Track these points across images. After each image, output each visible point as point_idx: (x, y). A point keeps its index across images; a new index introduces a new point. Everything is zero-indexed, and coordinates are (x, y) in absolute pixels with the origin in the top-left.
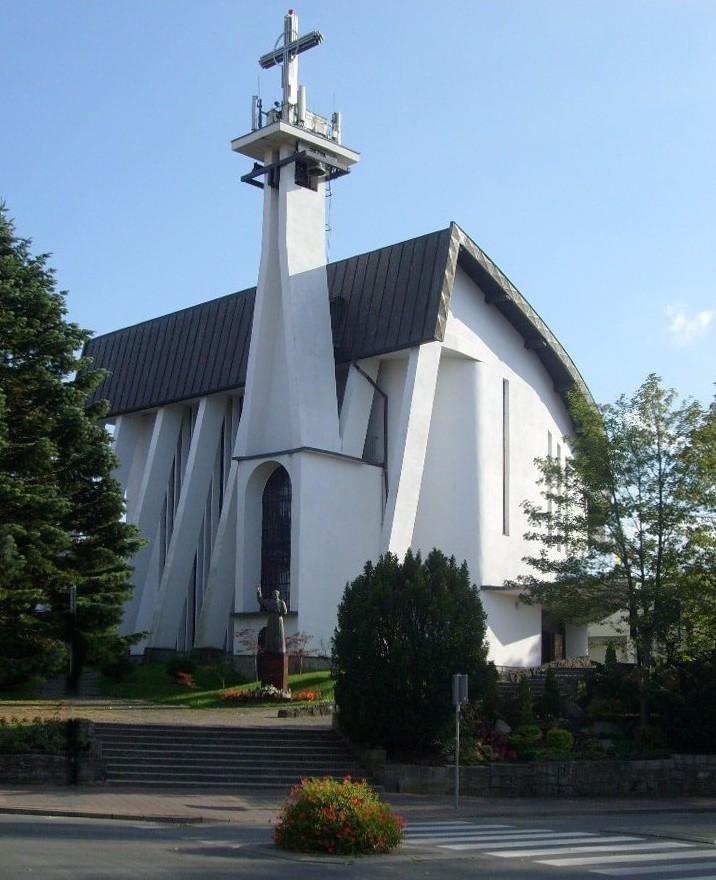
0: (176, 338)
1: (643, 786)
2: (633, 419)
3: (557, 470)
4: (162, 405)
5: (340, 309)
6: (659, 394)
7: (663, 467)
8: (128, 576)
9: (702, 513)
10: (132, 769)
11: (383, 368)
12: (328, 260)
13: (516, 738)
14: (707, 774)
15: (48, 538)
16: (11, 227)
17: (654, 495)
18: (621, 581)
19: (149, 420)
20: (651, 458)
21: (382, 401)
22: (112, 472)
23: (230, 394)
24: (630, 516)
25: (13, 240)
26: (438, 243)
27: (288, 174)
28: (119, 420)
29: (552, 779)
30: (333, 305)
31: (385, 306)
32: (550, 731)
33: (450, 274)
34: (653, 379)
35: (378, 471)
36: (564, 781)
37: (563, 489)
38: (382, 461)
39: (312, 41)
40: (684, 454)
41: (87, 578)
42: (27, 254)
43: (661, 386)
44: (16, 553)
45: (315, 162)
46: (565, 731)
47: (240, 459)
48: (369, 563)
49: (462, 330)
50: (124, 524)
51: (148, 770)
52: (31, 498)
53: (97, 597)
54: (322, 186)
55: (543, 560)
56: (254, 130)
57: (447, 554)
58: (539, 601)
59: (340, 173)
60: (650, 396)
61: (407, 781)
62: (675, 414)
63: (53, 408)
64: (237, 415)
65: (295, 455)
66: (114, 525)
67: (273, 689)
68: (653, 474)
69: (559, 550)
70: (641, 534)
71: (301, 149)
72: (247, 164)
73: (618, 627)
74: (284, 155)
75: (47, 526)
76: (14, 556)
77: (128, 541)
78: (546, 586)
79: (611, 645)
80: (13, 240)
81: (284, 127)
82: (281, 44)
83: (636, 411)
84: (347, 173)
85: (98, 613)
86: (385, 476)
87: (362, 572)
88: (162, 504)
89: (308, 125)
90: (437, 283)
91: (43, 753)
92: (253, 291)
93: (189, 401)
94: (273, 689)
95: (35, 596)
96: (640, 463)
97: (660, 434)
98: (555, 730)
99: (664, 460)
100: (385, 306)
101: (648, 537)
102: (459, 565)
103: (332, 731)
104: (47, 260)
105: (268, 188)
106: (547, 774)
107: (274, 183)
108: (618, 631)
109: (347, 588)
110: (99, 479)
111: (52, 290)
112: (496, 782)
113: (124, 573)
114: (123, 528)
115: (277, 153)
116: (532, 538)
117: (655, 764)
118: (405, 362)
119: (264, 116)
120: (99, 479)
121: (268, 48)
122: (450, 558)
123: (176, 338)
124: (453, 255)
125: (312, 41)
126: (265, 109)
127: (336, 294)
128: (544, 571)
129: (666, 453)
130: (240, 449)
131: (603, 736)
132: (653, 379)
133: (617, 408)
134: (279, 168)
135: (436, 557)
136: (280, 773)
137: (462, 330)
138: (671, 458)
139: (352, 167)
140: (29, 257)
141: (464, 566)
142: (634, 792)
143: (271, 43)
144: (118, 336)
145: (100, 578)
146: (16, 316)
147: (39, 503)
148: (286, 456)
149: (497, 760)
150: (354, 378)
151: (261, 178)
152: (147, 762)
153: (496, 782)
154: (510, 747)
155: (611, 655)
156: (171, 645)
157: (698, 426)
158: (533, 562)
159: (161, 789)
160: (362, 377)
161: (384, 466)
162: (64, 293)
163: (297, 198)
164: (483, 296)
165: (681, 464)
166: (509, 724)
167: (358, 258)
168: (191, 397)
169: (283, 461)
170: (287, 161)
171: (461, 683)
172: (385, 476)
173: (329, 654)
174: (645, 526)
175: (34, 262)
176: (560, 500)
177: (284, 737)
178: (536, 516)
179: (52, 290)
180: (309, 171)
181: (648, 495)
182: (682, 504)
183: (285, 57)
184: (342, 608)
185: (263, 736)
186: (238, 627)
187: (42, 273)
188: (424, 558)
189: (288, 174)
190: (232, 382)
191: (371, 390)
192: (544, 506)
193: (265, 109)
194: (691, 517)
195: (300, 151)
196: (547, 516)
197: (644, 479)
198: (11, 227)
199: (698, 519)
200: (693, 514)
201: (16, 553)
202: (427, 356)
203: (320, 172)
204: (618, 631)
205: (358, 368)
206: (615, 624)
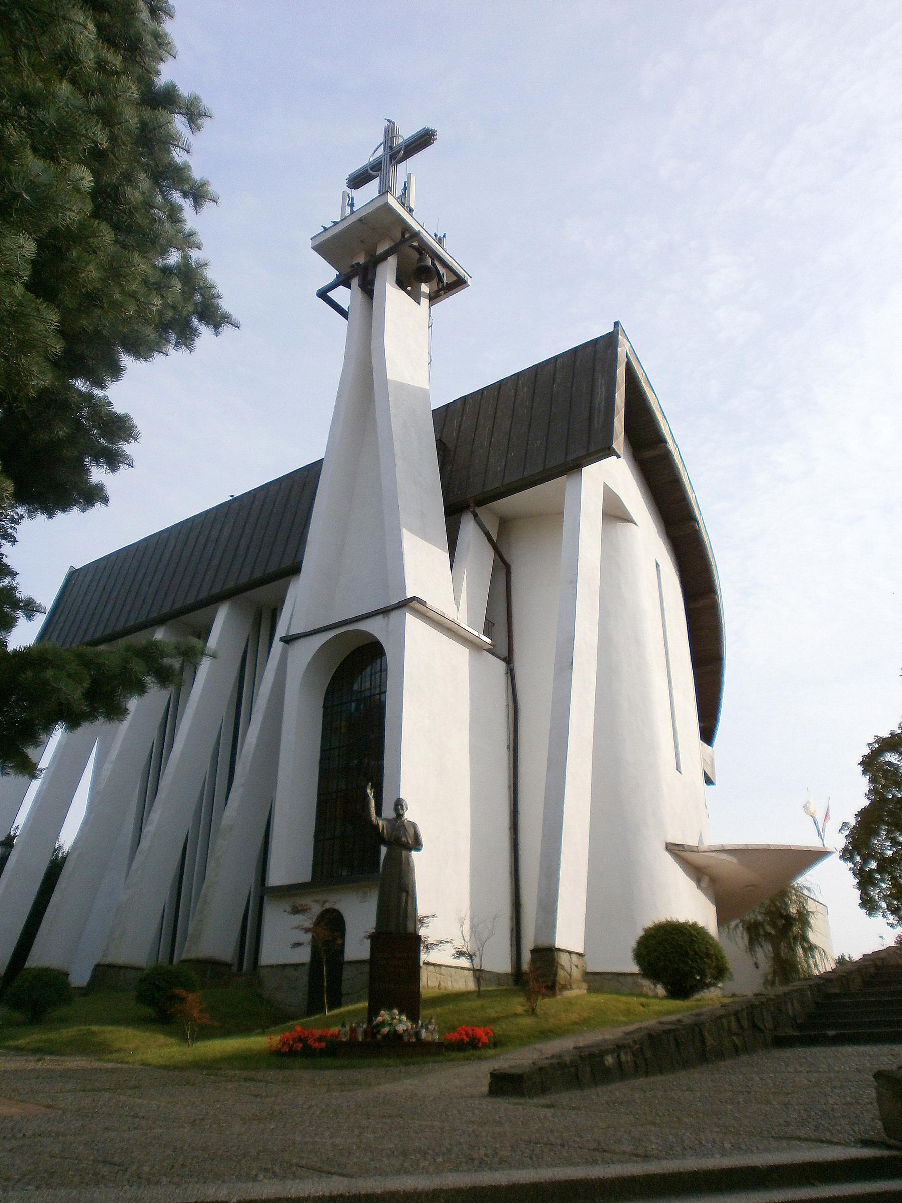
11: (505, 523)
12: (104, 955)
39: (424, 140)
49: (613, 475)
65: (394, 615)
82: (381, 152)
85: (872, 970)
86: (511, 673)
107: (368, 289)
125: (424, 140)
137: (613, 475)
143: (368, 151)
148: (379, 619)
150: (469, 530)
161: (508, 660)
169: (375, 627)
172: (511, 673)
189: (387, 272)
191: (489, 555)
205: (475, 516)
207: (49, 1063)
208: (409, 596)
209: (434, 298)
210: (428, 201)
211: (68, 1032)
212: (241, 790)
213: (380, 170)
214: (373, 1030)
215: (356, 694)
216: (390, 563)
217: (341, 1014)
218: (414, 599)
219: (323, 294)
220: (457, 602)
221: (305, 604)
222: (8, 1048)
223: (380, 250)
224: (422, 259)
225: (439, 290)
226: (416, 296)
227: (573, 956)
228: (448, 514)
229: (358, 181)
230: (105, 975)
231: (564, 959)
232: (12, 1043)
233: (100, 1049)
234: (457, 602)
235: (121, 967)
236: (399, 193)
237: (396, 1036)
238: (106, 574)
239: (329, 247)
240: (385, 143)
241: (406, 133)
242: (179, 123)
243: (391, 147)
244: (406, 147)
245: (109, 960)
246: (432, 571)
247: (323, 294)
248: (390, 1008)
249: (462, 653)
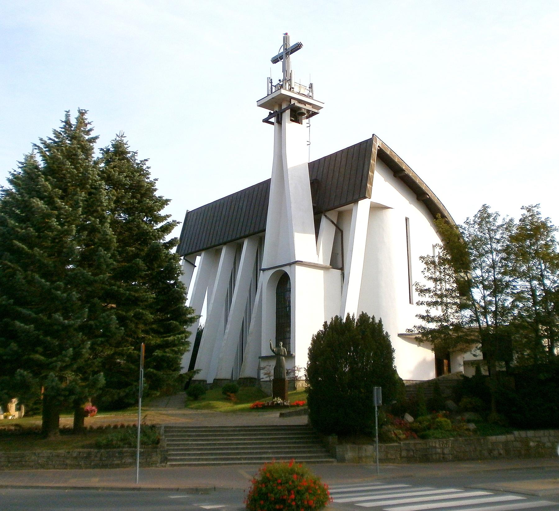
1: (496, 453)
2: (474, 230)
3: (433, 263)
4: (225, 244)
5: (316, 185)
6: (489, 216)
7: (494, 258)
8: (186, 337)
9: (520, 283)
10: (185, 455)
11: (340, 215)
13: (416, 425)
14: (536, 443)
15: (138, 317)
16: (127, 146)
17: (490, 274)
18: (475, 325)
19: (218, 252)
20: (487, 252)
22: (179, 278)
23: (258, 235)
24: (478, 287)
25: (129, 153)
26: (366, 146)
27: (287, 115)
28: (203, 254)
29: (439, 451)
30: (312, 183)
31: (339, 184)
32: (437, 420)
33: (374, 161)
34: (485, 207)
35: (339, 272)
36: (446, 451)
37: (438, 273)
38: (340, 266)
39: (298, 47)
40: (507, 250)
41: (162, 339)
42: (136, 160)
43: (490, 211)
44: (118, 326)
45: (300, 108)
46: (446, 419)
47: (264, 270)
48: (326, 323)
50: (517, 367)
51: (194, 455)
52: (130, 294)
53: (167, 350)
54: (305, 121)
55: (428, 316)
56: (268, 95)
57: (370, 315)
58: (427, 340)
59: (314, 114)
60: (484, 217)
61: (349, 455)
62: (498, 227)
63: (145, 242)
65: (293, 266)
66: (179, 307)
67: (280, 401)
68: (489, 262)
69: (437, 309)
70: (484, 297)
71: (293, 102)
72: (266, 113)
73: (474, 353)
74: (284, 107)
75: (138, 310)
76: (116, 328)
77: (189, 316)
78: (432, 331)
79: (59, 316)
80: (129, 153)
81: (283, 92)
82: (282, 50)
83: (477, 226)
84: (318, 113)
87: (322, 328)
88: (246, 303)
89: (296, 89)
90: (366, 167)
91: (130, 447)
93: (239, 241)
94: (280, 401)
95: (130, 351)
96: (481, 255)
97: (491, 238)
98: (439, 419)
99: (494, 253)
100: (339, 184)
101: (489, 298)
102: (377, 321)
103: (307, 425)
104: (147, 162)
105: (276, 124)
106: (435, 447)
107: (279, 122)
108: (474, 355)
109: (313, 338)
110: (172, 282)
111: (148, 178)
112: (404, 454)
113: (184, 335)
114: (185, 309)
115: (280, 106)
116: (421, 304)
117: (502, 438)
118: (350, 211)
119: (274, 88)
120: (172, 282)
121: (275, 53)
122: (371, 317)
124: (375, 151)
125: (298, 47)
126: (274, 84)
127: (314, 178)
128: (429, 322)
129: (495, 250)
130: (265, 265)
131: (469, 421)
132: (485, 207)
133: (464, 225)
134: (281, 114)
135: (364, 317)
136: (273, 453)
138: (498, 252)
139: (320, 111)
140: (136, 161)
141: (380, 321)
142: (490, 456)
145: (169, 338)
146: (125, 193)
147: (134, 296)
149: (405, 439)
150: (324, 223)
151: (273, 120)
152: (194, 449)
153: (404, 454)
154: (416, 431)
155: (478, 370)
156: (228, 376)
157: (513, 232)
158: (423, 317)
161: (342, 269)
162: (156, 180)
163: (290, 126)
164: (392, 173)
165: (504, 255)
166: (413, 416)
167: (325, 158)
168: (238, 239)
170: (285, 109)
171: (377, 393)
173: (197, 377)
174: (487, 293)
175: (139, 164)
176: (435, 280)
177: (278, 430)
178: (423, 291)
179: (148, 178)
180: (297, 116)
181: (487, 274)
182: (507, 278)
183: (284, 57)
184: (310, 350)
185: (267, 430)
186: (263, 364)
187: (143, 170)
188: (356, 317)
189: (287, 115)
191: (333, 229)
192: (430, 285)
193: (274, 84)
194: (514, 286)
195: (292, 103)
196: (428, 290)
197: (484, 265)
198: (127, 146)
199: (518, 287)
200: (514, 284)
201: (118, 326)
202: (363, 206)
203: (304, 114)
204: (474, 355)
205: (326, 216)
206: (475, 353)
207: (199, 411)
210: (304, 73)
211: (204, 403)
212: (254, 319)
214: (273, 403)
216: (290, 246)
217: (136, 457)
220: (318, 254)
222: (189, 408)
230: (217, 381)
232: (190, 406)
233: (212, 407)
234: (318, 254)
235: (222, 380)
237: (278, 404)
238: (202, 216)
240: (284, 45)
241: (292, 43)
242: (184, 295)
243: (286, 49)
245: (218, 378)
246: (307, 246)
248: (277, 397)
249: (321, 272)
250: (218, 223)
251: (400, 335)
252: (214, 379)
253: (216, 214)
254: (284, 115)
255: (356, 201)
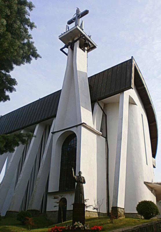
0: (30, 110)
11: (105, 105)
21: (105, 118)
27: (77, 44)
39: (86, 12)
49: (131, 93)
64: (48, 135)
65: (79, 127)
82: (75, 16)
86: (107, 141)
92: (58, 93)
121: (71, 18)
123: (30, 110)
125: (86, 12)
137: (131, 93)
143: (72, 15)
144: (6, 116)
148: (75, 128)
150: (96, 106)
159: (108, 207)
160: (99, 107)
161: (106, 138)
172: (107, 141)
189: (77, 44)
190: (53, 114)
205: (98, 103)
208: (82, 122)
209: (88, 51)
210: (88, 28)
213: (75, 20)
215: (70, 145)
218: (84, 123)
219: (61, 50)
221: (57, 125)
223: (75, 39)
224: (85, 41)
225: (90, 49)
226: (84, 50)
227: (122, 209)
228: (92, 102)
229: (70, 22)
231: (119, 210)
234: (94, 124)
235: (13, 212)
236: (80, 25)
239: (63, 38)
240: (76, 14)
241: (82, 11)
242: (27, 9)
244: (82, 14)
245: (10, 210)
247: (61, 50)
249: (95, 136)
250: (20, 118)
251: (145, 183)
252: (7, 211)
253: (19, 114)
254: (75, 44)
255: (122, 91)
